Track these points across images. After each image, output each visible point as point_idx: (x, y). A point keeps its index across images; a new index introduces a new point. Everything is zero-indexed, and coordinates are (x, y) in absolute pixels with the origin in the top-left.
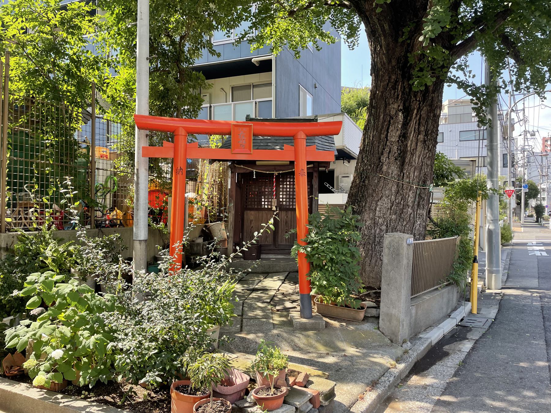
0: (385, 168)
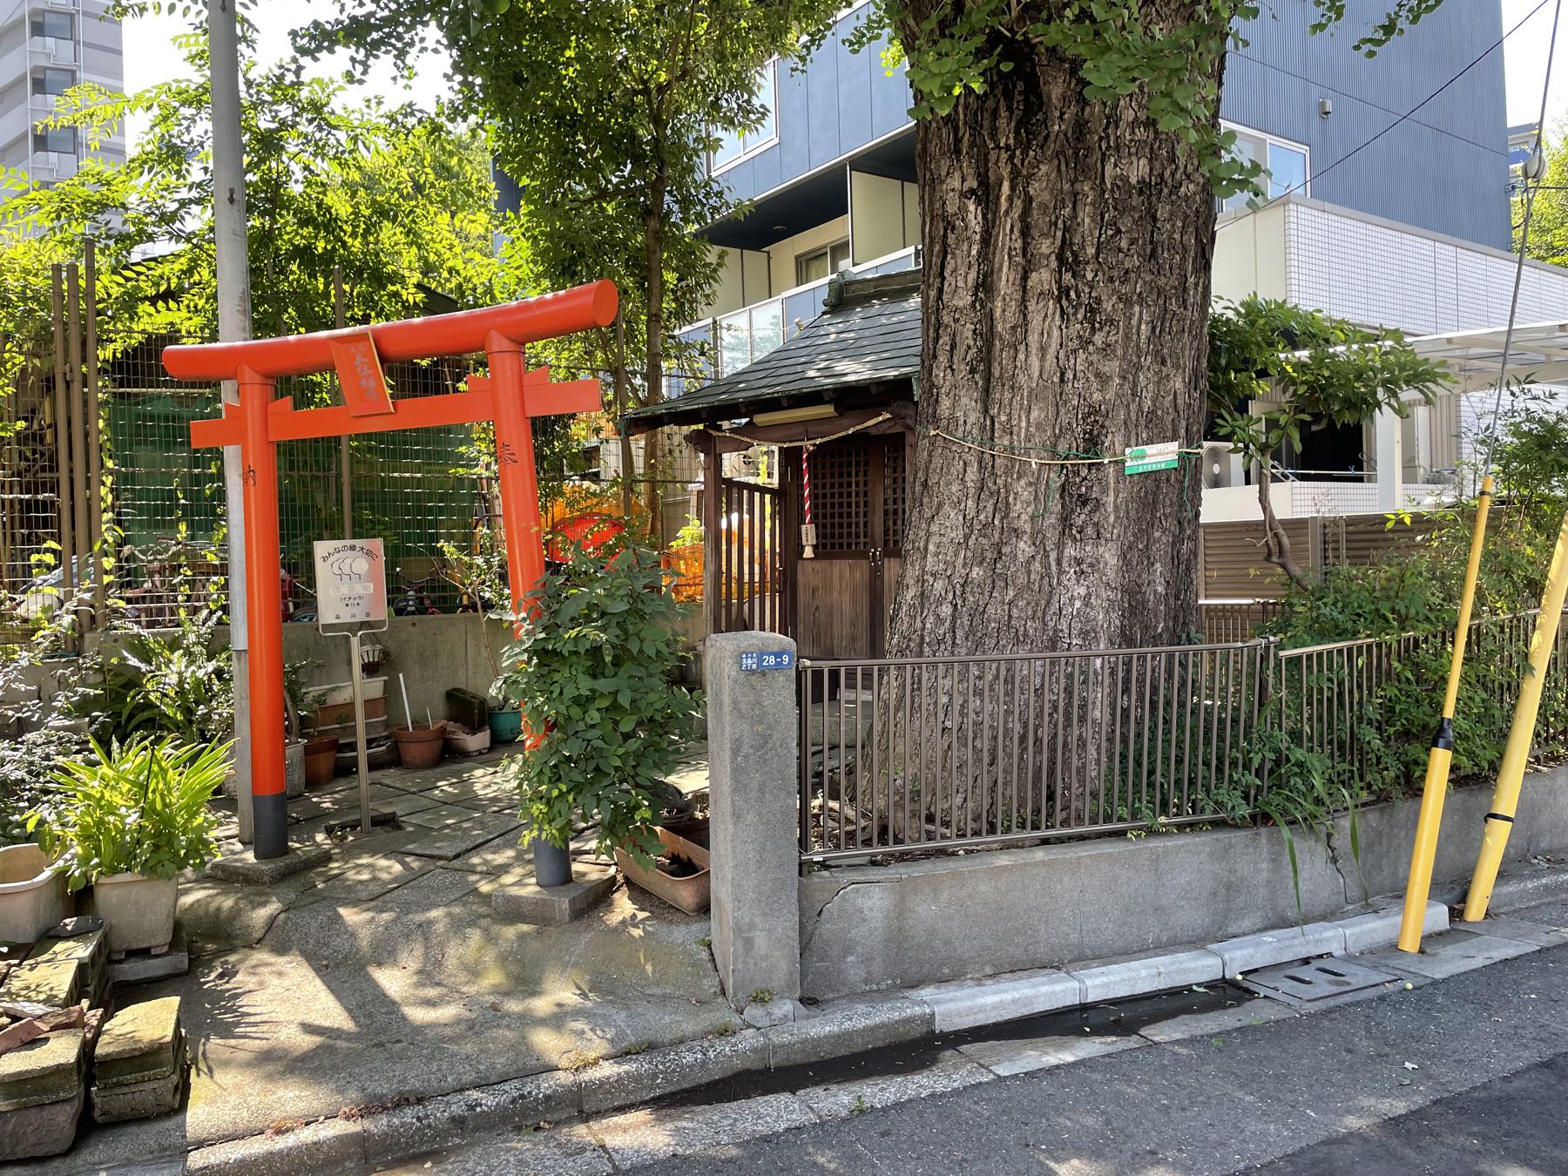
0: (945, 403)
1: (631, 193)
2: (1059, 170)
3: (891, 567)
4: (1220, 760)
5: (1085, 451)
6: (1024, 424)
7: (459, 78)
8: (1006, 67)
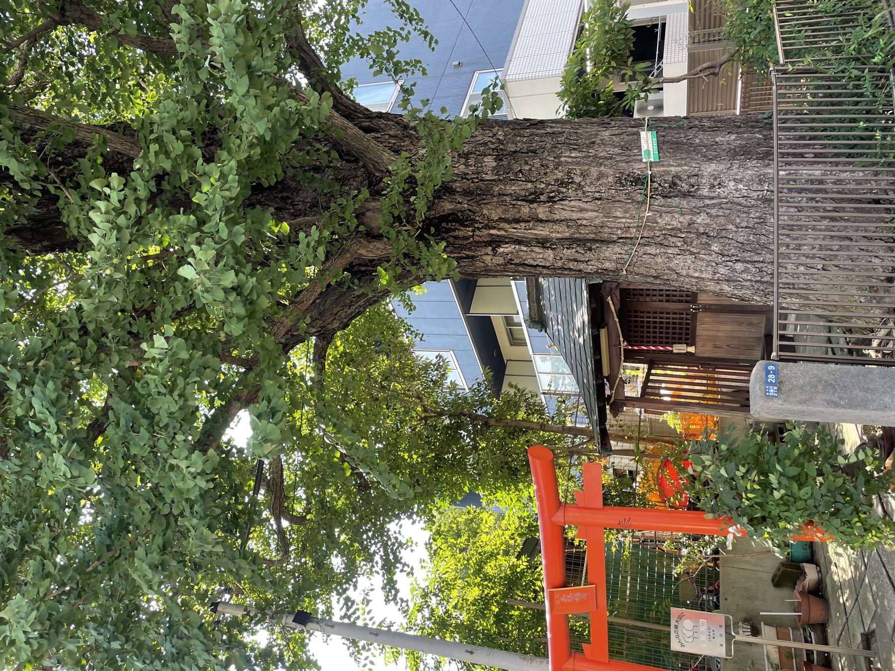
0: (607, 265)
1: (476, 432)
2: (487, 204)
3: (703, 299)
4: (856, 95)
5: (643, 184)
6: (624, 220)
7: (414, 516)
8: (433, 230)
